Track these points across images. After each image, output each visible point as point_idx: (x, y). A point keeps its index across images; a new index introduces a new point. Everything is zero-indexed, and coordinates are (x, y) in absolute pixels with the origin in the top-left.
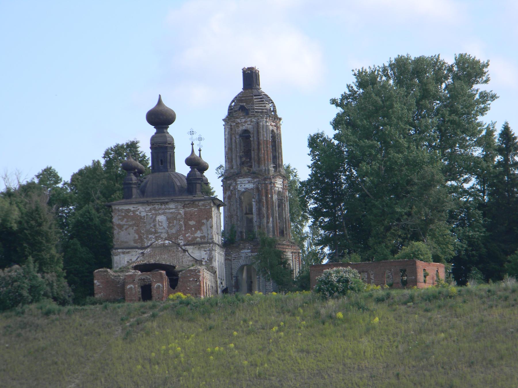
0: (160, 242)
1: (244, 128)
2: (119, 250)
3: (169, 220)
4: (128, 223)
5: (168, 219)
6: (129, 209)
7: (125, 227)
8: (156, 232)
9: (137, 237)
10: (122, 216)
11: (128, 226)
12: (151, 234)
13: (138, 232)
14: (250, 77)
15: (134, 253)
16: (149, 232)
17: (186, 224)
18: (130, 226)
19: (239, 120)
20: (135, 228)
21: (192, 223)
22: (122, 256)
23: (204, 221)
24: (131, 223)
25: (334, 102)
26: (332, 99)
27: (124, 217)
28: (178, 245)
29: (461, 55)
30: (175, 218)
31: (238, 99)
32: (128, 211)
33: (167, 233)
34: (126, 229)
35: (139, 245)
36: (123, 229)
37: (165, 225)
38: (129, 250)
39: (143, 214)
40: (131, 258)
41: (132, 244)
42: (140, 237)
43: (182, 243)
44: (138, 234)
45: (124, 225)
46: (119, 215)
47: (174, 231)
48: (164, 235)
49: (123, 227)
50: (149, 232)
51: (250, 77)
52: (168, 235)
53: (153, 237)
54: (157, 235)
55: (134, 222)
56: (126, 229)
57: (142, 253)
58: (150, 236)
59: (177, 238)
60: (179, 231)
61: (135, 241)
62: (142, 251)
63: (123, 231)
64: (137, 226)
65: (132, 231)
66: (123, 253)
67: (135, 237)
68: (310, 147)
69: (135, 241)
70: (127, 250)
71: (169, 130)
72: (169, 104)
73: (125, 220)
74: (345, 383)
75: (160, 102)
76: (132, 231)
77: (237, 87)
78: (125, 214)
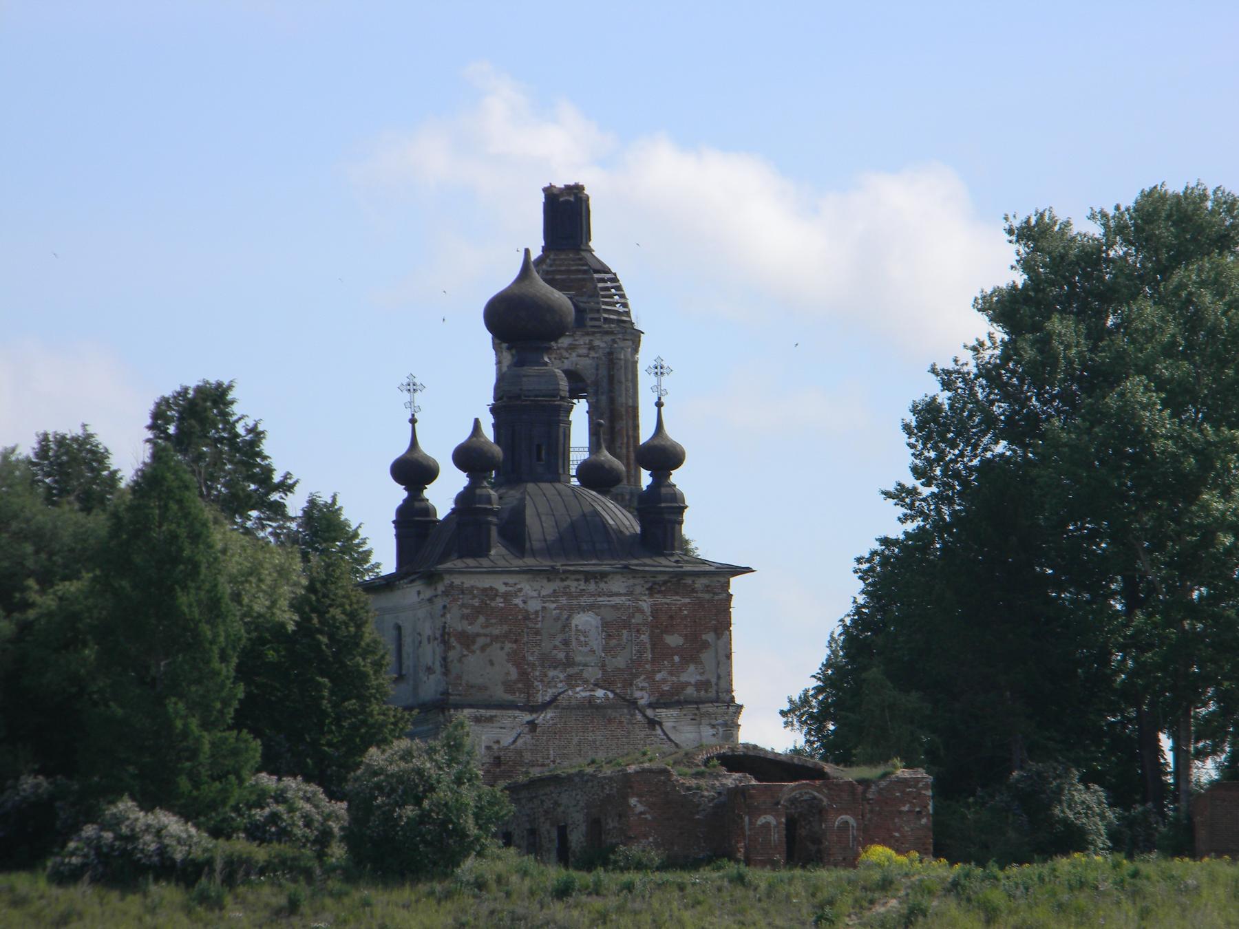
0: (581, 693)
5: (605, 624)
8: (569, 662)
13: (517, 659)
16: (548, 661)
17: (656, 642)
21: (673, 640)
28: (633, 704)
30: (626, 624)
39: (534, 605)
42: (524, 676)
43: (643, 698)
47: (620, 661)
48: (593, 673)
50: (548, 661)
57: (532, 725)
59: (629, 684)
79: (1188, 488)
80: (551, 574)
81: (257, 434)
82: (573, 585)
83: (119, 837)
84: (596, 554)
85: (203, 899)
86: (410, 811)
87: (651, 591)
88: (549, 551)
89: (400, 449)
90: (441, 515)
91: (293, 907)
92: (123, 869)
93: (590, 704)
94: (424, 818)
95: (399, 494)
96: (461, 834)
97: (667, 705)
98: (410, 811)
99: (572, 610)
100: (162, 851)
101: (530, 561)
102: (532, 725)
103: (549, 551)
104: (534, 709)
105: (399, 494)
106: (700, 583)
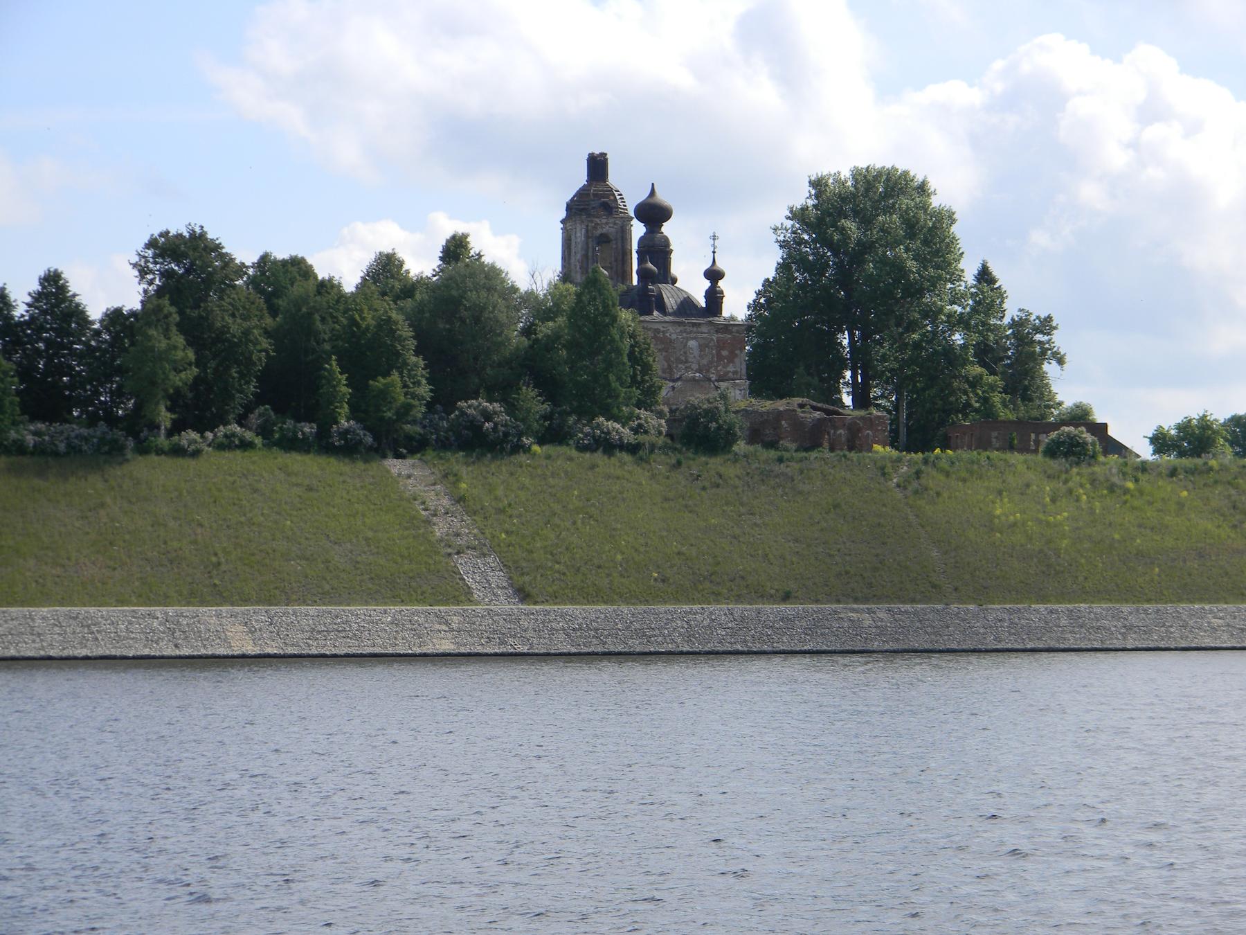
0: (690, 374)
1: (604, 231)
3: (702, 347)
5: (700, 346)
8: (686, 362)
13: (667, 359)
14: (597, 166)
16: (679, 361)
17: (719, 354)
19: (598, 220)
21: (725, 353)
23: (737, 352)
28: (709, 380)
30: (707, 346)
31: (582, 194)
37: (696, 353)
39: (674, 337)
42: (670, 367)
43: (714, 377)
47: (705, 362)
48: (695, 366)
50: (679, 361)
51: (597, 166)
57: (673, 388)
59: (708, 371)
60: (711, 362)
68: (41, 284)
71: (663, 229)
72: (663, 197)
75: (653, 192)
77: (579, 177)
79: (921, 292)
80: (679, 324)
81: (184, 265)
82: (688, 329)
83: (602, 432)
84: (692, 315)
85: (641, 459)
86: (714, 425)
87: (717, 332)
88: (675, 314)
89: (708, 265)
90: (20, 311)
91: (679, 463)
92: (607, 445)
93: (694, 379)
94: (719, 428)
95: (707, 284)
96: (735, 435)
97: (723, 381)
98: (714, 425)
99: (688, 339)
100: (621, 439)
101: (668, 319)
102: (673, 388)
103: (675, 314)
104: (674, 381)
105: (707, 284)
106: (735, 329)
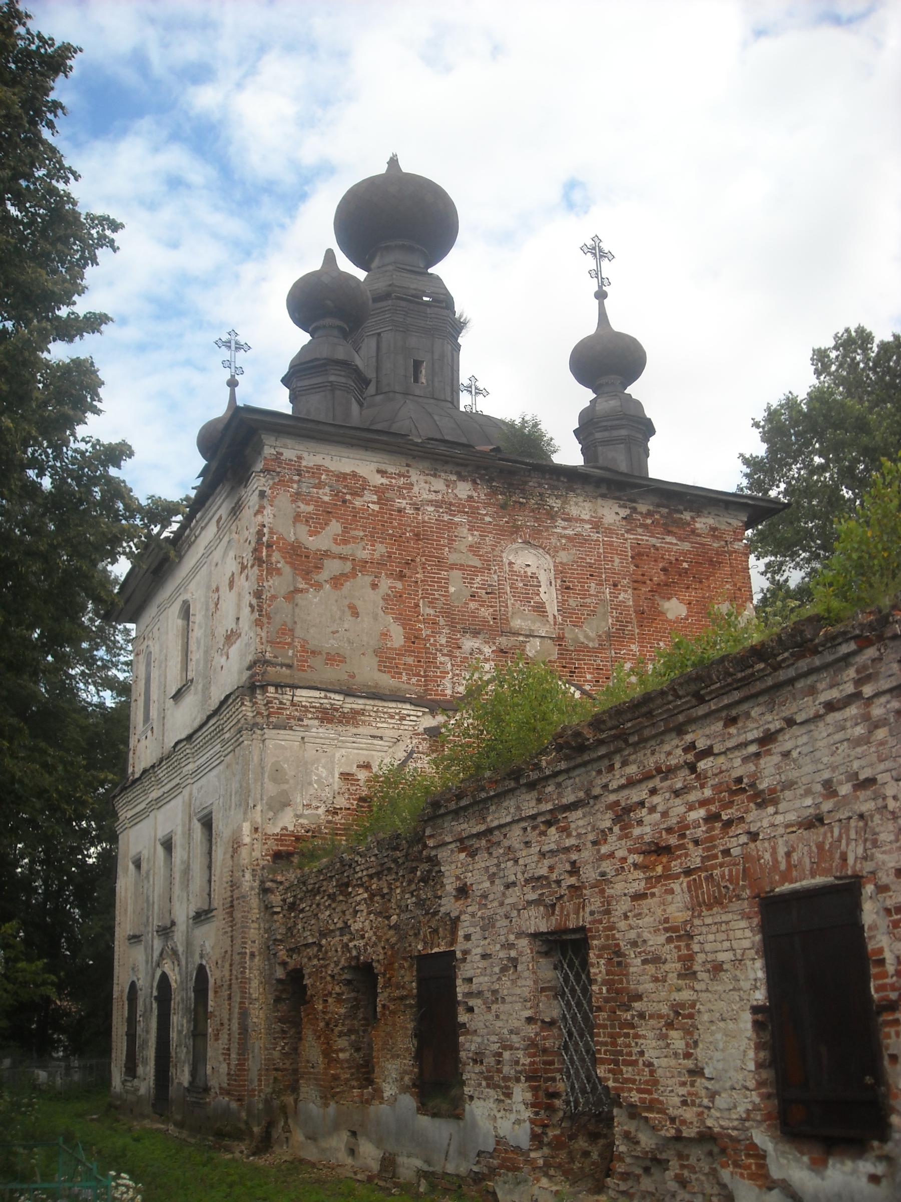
2: (304, 696)
4: (346, 550)
5: (561, 571)
6: (354, 475)
7: (332, 567)
9: (398, 637)
10: (318, 501)
11: (348, 566)
12: (476, 634)
13: (400, 606)
15: (386, 728)
18: (362, 566)
20: (385, 584)
22: (318, 731)
24: (363, 554)
25: (894, 335)
26: (819, 350)
27: (327, 512)
29: (772, 415)
32: (354, 484)
33: (559, 640)
34: (337, 581)
35: (408, 684)
36: (324, 575)
38: (358, 704)
40: (364, 756)
41: (368, 671)
44: (404, 621)
45: (327, 554)
46: (297, 497)
49: (319, 568)
52: (563, 652)
53: (487, 650)
54: (503, 641)
55: (381, 549)
56: (337, 581)
58: (469, 644)
61: (387, 660)
62: (429, 722)
63: (318, 586)
64: (401, 576)
65: (369, 595)
66: (327, 716)
67: (385, 635)
69: (387, 660)
70: (352, 704)
73: (335, 527)
74: (307, 946)
76: (369, 595)
78: (336, 494)
